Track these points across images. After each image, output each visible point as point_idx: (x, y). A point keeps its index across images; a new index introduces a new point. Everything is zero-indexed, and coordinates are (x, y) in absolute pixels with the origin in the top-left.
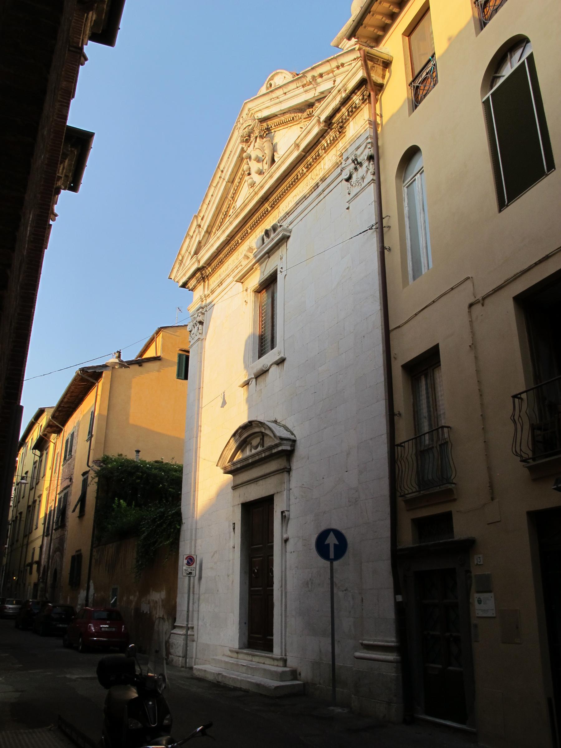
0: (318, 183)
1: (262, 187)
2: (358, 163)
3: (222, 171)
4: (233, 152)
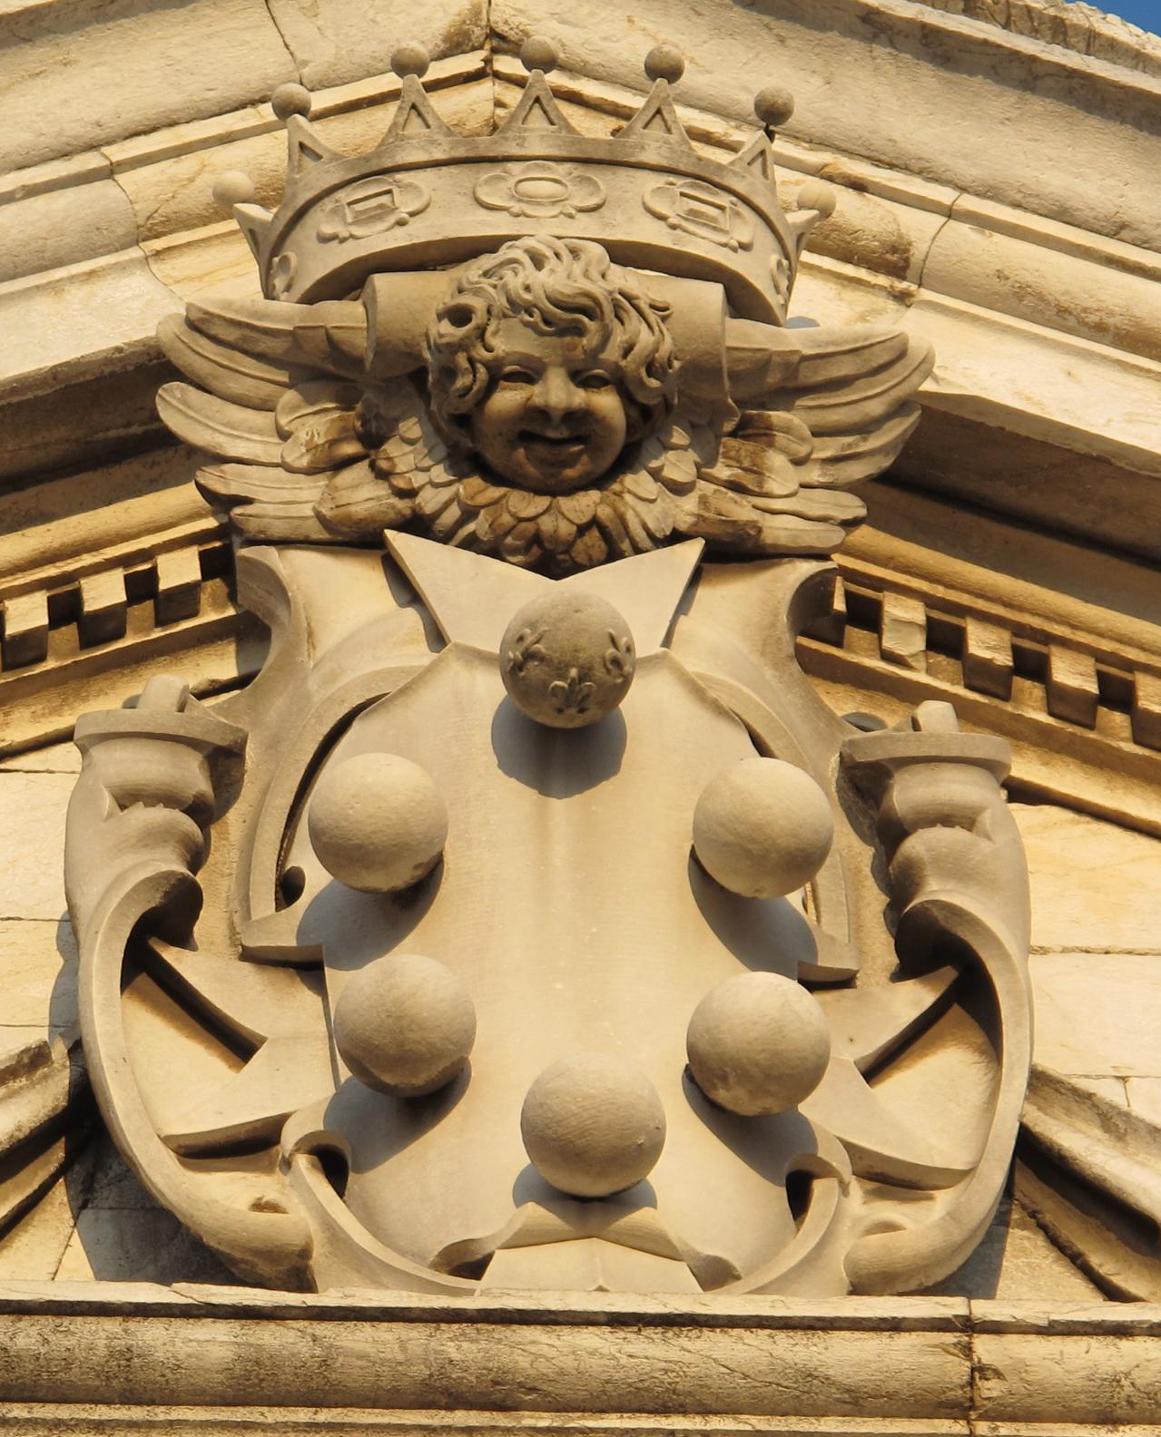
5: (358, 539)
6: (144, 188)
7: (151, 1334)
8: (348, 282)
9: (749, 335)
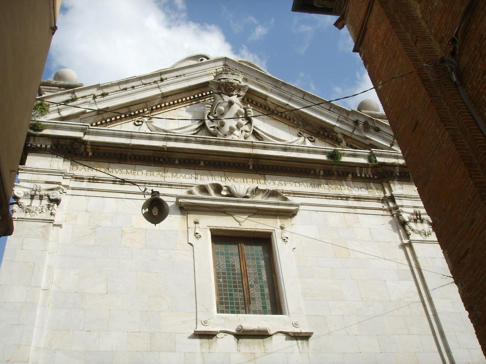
0: (349, 197)
1: (265, 148)
2: (420, 219)
3: (162, 80)
4: (187, 77)
5: (219, 94)
6: (208, 72)
7: (211, 140)
8: (220, 80)
9: (240, 84)
